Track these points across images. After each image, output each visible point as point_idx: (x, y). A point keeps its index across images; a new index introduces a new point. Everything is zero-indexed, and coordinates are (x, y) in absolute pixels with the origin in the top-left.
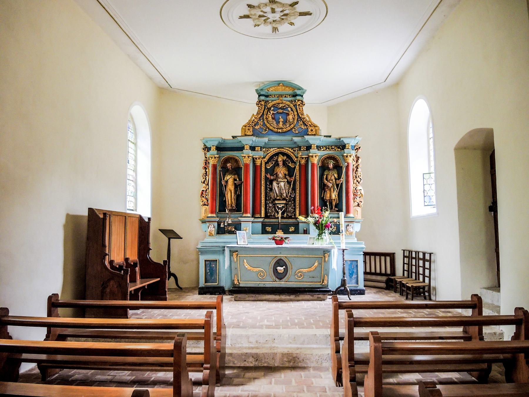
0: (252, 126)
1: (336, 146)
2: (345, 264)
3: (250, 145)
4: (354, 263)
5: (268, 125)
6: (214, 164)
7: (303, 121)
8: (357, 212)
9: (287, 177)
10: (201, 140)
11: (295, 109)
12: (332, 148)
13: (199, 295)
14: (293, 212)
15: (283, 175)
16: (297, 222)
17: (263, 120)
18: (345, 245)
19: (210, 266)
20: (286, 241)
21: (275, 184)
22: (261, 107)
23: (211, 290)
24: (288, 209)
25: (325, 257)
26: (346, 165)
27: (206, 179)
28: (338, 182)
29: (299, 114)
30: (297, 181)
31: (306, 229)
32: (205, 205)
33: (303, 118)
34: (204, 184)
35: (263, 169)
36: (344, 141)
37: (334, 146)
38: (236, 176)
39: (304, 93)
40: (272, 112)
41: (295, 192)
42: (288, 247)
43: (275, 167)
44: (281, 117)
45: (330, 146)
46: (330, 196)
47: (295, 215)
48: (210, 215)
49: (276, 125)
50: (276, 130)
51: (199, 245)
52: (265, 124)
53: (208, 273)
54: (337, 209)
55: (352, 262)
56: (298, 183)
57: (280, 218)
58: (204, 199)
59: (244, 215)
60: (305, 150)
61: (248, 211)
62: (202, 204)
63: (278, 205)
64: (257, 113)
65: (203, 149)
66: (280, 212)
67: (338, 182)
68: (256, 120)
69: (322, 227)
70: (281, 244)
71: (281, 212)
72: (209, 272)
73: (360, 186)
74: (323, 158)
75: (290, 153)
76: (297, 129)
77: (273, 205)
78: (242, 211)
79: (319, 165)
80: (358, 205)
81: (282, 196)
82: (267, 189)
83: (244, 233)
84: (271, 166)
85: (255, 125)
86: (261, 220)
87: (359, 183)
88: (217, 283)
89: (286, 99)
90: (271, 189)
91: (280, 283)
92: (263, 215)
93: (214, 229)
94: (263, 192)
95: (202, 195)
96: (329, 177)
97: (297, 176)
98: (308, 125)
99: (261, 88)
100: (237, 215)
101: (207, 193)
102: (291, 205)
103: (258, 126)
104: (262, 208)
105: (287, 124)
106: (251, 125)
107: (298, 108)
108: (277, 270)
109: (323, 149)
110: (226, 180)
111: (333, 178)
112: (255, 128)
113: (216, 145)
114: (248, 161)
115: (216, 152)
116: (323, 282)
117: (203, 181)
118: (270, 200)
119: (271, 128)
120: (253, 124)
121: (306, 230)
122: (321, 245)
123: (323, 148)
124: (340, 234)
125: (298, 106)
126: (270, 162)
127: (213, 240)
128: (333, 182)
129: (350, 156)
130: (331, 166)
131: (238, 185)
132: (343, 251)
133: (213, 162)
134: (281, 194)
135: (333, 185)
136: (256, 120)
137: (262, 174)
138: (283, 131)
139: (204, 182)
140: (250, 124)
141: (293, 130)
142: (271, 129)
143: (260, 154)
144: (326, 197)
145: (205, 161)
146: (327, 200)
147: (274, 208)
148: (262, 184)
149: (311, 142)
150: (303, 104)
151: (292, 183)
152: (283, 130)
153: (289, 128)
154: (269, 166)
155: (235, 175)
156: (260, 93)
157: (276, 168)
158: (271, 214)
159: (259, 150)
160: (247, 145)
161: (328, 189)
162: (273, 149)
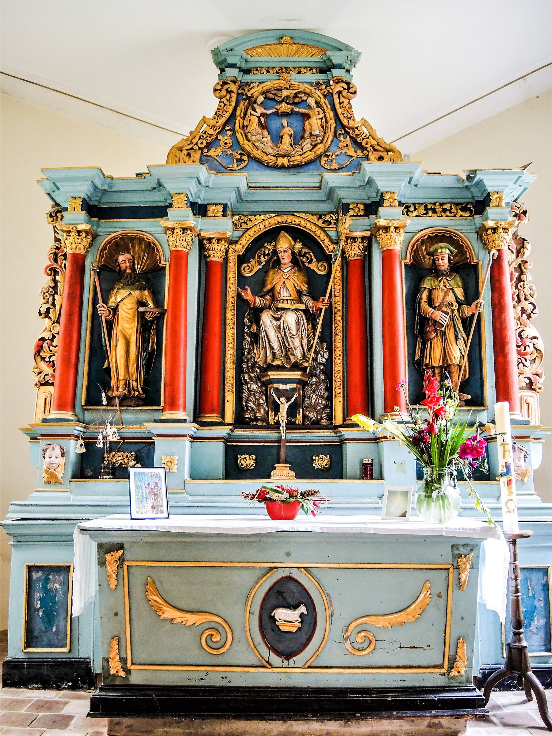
0: (200, 148)
1: (457, 204)
2: (519, 587)
3: (191, 200)
4: (536, 577)
5: (248, 146)
6: (77, 251)
7: (351, 137)
8: (526, 406)
9: (304, 299)
10: (38, 182)
11: (327, 103)
12: (444, 210)
13: (6, 689)
14: (324, 409)
15: (294, 295)
16: (337, 439)
17: (234, 134)
18: (519, 515)
19: (45, 587)
20: (309, 505)
21: (266, 318)
22: (228, 97)
23: (45, 671)
24: (309, 398)
25: (458, 568)
26: (495, 258)
27: (53, 304)
28: (468, 311)
29: (341, 117)
30: (335, 313)
31: (370, 462)
32: (46, 384)
33: (353, 129)
34: (47, 319)
35: (232, 276)
36: (485, 182)
37: (449, 203)
38: (146, 292)
39: (353, 63)
40: (260, 110)
41: (330, 349)
42: (319, 530)
43: (267, 272)
44: (285, 124)
45: (438, 204)
46: (445, 355)
47: (330, 417)
48: (54, 414)
49: (271, 144)
50: (270, 159)
51: (9, 515)
52: (239, 143)
53: (38, 610)
54: (469, 397)
55: (527, 574)
56: (340, 318)
57: (283, 424)
58: (43, 366)
59: (167, 415)
60: (360, 216)
61: (181, 402)
62: (36, 379)
63: (276, 386)
64: (216, 114)
65: (51, 216)
66: (284, 407)
67: (468, 311)
68: (211, 131)
69: (442, 455)
70: (289, 514)
71: (287, 405)
72: (40, 608)
73: (531, 325)
74: (418, 240)
75: (314, 228)
76: (334, 157)
77: (261, 386)
78: (162, 404)
79: (406, 259)
80: (530, 385)
81: (291, 357)
82: (244, 338)
83: (156, 476)
84: (255, 270)
85: (209, 146)
86: (223, 431)
87: (529, 317)
88: (64, 646)
89: (301, 78)
90: (256, 338)
91: (288, 670)
92: (230, 417)
93: (61, 460)
94: (231, 345)
95: (39, 351)
96: (439, 296)
97: (335, 296)
98: (367, 146)
99: (229, 47)
100: (143, 416)
101: (56, 346)
102: (317, 386)
103: (216, 149)
104: (227, 393)
105: (305, 143)
106: (196, 144)
107: (337, 101)
108: (273, 619)
109: (415, 213)
110: (114, 304)
111: (451, 298)
112: (210, 154)
113: (83, 195)
114: (183, 243)
115: (82, 215)
116: (451, 668)
117: (43, 310)
118: (253, 371)
119: (257, 153)
120: (202, 143)
121: (372, 465)
122: (441, 522)
123: (415, 210)
124: (499, 481)
125: (336, 97)
126: (254, 258)
127: (58, 498)
128: (453, 310)
129: (504, 229)
130: (444, 263)
131: (152, 322)
132: (514, 542)
133: (74, 246)
134: (287, 350)
135: (452, 319)
136: (211, 131)
137: (228, 289)
138: (292, 163)
139: (47, 314)
140: (195, 141)
141: (324, 159)
142: (257, 156)
143: (221, 229)
144: (430, 358)
145: (54, 250)
146: (433, 368)
147: (264, 397)
148: (228, 321)
149: (382, 185)
150: (351, 90)
151: (320, 321)
152: (292, 159)
153: (309, 153)
154: (251, 271)
155: (141, 289)
156: (225, 60)
157: (271, 273)
158: (255, 414)
159: (218, 215)
160: (179, 194)
161: (437, 334)
162: (263, 217)
